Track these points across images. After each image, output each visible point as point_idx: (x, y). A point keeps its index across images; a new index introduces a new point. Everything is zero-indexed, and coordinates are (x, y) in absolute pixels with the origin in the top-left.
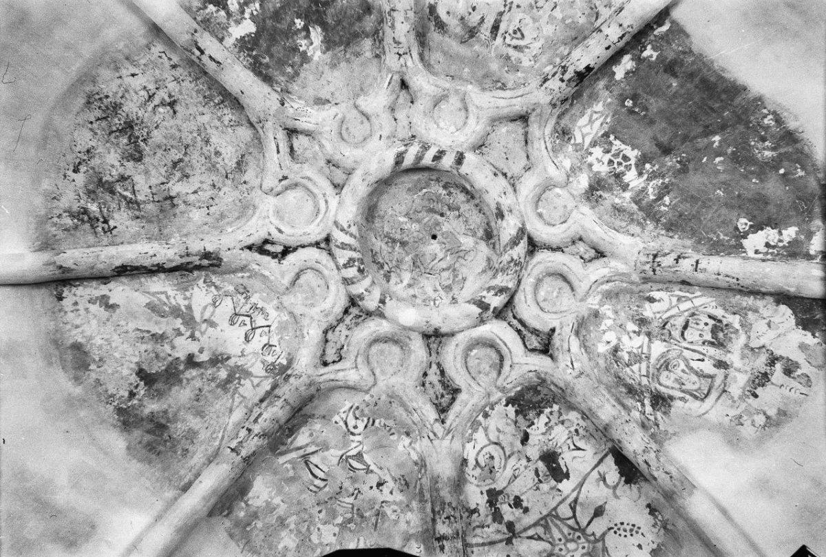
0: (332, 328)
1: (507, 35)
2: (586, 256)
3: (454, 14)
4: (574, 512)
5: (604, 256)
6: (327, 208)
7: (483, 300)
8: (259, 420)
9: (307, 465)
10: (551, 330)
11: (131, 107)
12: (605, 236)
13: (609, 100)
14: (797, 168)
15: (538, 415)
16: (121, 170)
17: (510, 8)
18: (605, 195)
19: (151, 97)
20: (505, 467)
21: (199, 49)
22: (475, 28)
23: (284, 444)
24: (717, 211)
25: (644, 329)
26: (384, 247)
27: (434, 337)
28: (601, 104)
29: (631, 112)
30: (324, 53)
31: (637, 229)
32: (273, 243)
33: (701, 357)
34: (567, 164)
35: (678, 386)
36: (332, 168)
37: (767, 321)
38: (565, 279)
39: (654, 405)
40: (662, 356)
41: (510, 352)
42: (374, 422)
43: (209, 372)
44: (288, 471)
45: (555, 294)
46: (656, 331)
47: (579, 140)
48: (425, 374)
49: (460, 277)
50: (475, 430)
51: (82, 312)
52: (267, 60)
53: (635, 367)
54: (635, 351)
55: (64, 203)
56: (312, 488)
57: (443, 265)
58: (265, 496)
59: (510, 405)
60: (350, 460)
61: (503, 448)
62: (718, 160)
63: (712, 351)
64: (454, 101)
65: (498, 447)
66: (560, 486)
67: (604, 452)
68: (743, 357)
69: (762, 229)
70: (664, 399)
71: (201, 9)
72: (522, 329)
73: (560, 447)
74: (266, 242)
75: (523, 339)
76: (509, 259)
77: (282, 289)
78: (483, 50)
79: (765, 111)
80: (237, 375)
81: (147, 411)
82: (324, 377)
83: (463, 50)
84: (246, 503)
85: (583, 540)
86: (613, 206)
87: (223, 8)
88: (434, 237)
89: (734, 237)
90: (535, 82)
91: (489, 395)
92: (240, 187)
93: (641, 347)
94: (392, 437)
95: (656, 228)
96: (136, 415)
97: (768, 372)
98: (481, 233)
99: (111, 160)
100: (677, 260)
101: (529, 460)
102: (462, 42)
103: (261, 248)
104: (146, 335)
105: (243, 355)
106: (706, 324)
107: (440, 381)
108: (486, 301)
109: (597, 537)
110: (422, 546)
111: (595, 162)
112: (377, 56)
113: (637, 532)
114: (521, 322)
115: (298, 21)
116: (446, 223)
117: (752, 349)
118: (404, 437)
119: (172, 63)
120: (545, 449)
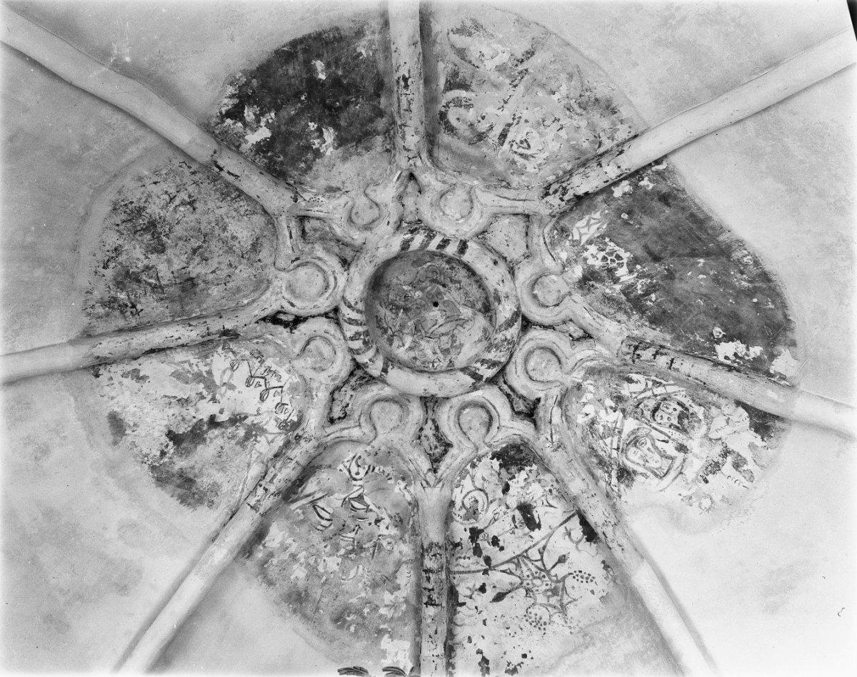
0: (338, 389)
1: (514, 143)
2: (575, 335)
3: (463, 120)
4: (542, 556)
5: (591, 338)
6: (336, 283)
7: (477, 371)
8: (275, 481)
9: (315, 509)
10: (537, 399)
11: (154, 209)
12: (593, 323)
13: (607, 211)
14: (767, 302)
15: (520, 470)
16: (146, 262)
17: (519, 121)
18: (597, 285)
19: (172, 199)
20: (487, 510)
21: (218, 167)
22: (483, 133)
23: (296, 493)
24: (697, 315)
25: (620, 406)
26: (388, 313)
27: (430, 402)
28: (598, 213)
29: (626, 223)
30: (337, 149)
31: (624, 318)
32: (285, 313)
33: (667, 438)
34: (564, 256)
35: (642, 463)
36: (341, 246)
37: (726, 418)
38: (553, 353)
39: (619, 478)
40: (633, 433)
41: (498, 415)
42: (374, 469)
43: (229, 430)
44: (299, 515)
45: (543, 365)
46: (629, 408)
47: (576, 237)
48: (421, 429)
49: (458, 343)
50: (464, 478)
51: (116, 384)
52: (282, 158)
53: (608, 441)
54: (610, 425)
55: (97, 294)
56: (319, 527)
57: (443, 330)
58: (279, 539)
59: (495, 459)
60: (352, 502)
61: (486, 494)
62: (701, 276)
63: (677, 435)
64: (460, 194)
65: (482, 493)
66: (532, 534)
67: (572, 513)
68: (702, 445)
69: (733, 341)
70: (628, 473)
71: (218, 124)
72: (511, 393)
73: (535, 502)
74: (279, 312)
75: (511, 402)
76: (503, 338)
77: (293, 356)
78: (490, 152)
79: (746, 252)
80: (254, 433)
81: (177, 468)
82: (332, 436)
83: (471, 151)
84: (264, 545)
85: (547, 579)
86: (603, 294)
87: (240, 120)
88: (436, 304)
89: (709, 340)
90: (536, 193)
91: (477, 449)
92: (255, 264)
93: (616, 422)
94: (389, 482)
95: (641, 318)
96: (168, 472)
97: (720, 462)
98: (479, 305)
99: (136, 254)
100: (655, 356)
101: (508, 507)
102: (470, 144)
103: (274, 319)
104: (173, 400)
105: (259, 414)
106: (675, 410)
107: (434, 435)
108: (480, 373)
109: (559, 579)
110: (412, 572)
111: (590, 257)
112: (388, 151)
113: (592, 581)
114: (510, 387)
115: (311, 124)
116: (448, 294)
117: (711, 439)
118: (400, 481)
119: (192, 170)
120: (522, 500)
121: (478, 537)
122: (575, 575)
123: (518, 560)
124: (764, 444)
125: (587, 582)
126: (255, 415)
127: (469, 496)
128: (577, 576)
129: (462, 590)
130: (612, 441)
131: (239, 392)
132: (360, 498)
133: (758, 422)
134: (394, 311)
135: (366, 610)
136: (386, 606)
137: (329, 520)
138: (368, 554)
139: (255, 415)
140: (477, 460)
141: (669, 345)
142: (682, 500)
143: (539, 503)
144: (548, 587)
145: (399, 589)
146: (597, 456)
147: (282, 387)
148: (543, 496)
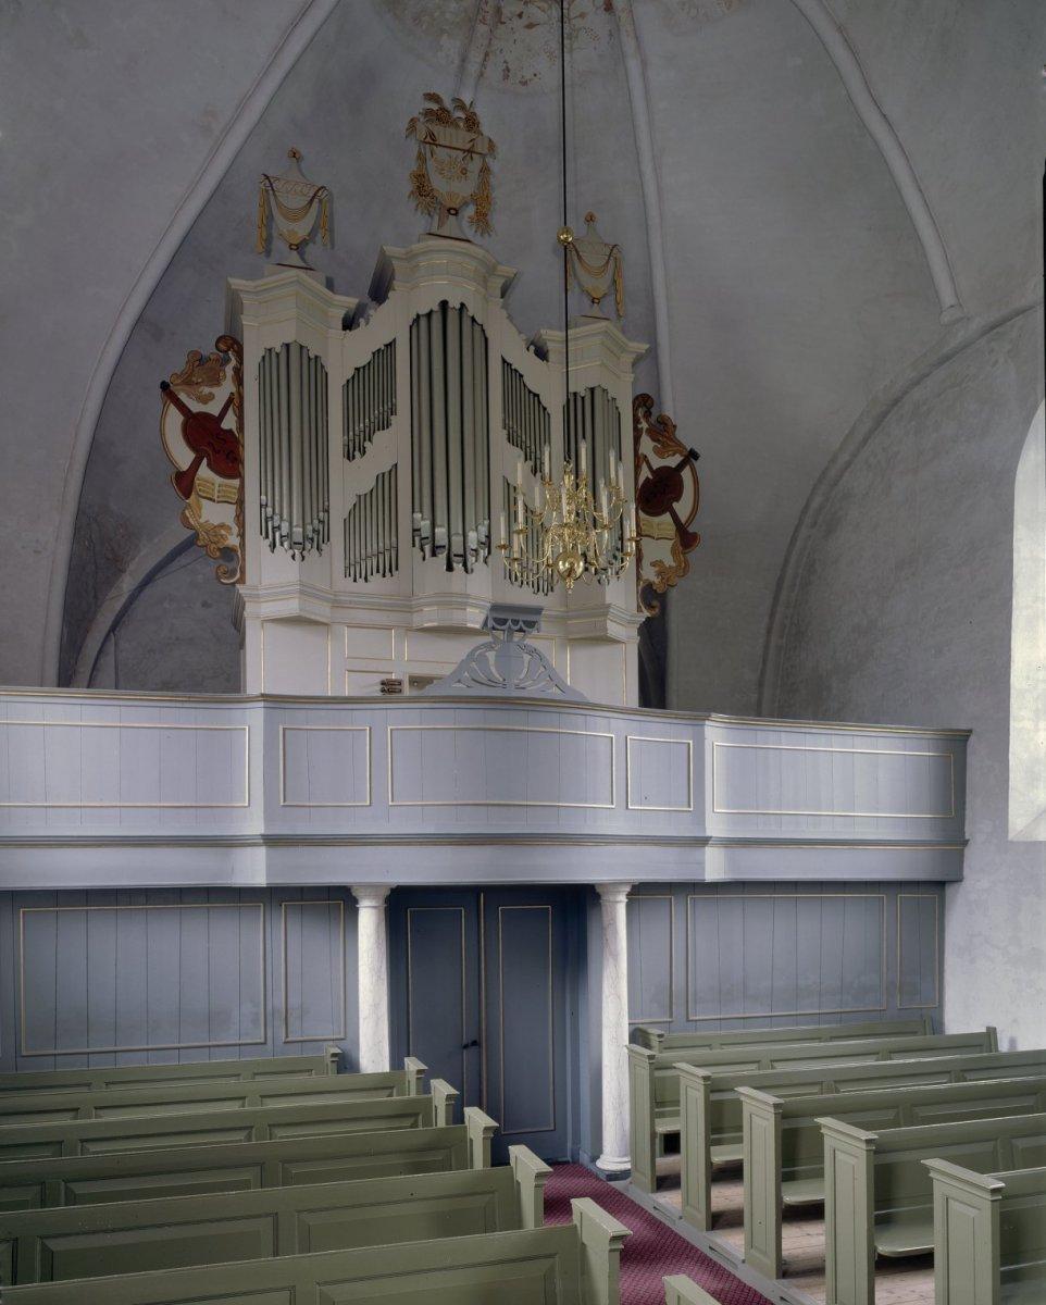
129: (506, 12)
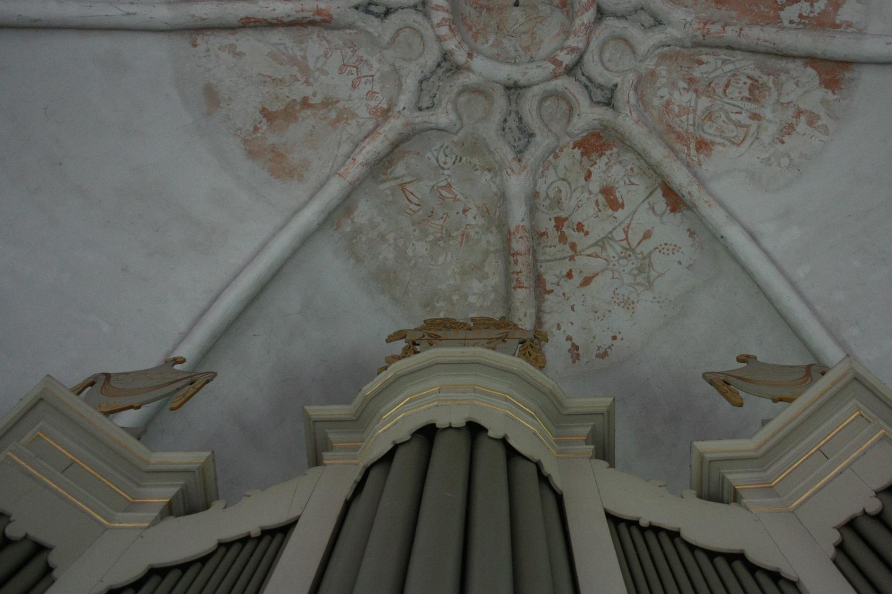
4: (627, 236)
9: (404, 191)
10: (614, 85)
15: (600, 156)
20: (570, 199)
25: (693, 87)
27: (513, 89)
33: (740, 110)
39: (698, 149)
42: (461, 159)
43: (321, 112)
48: (505, 121)
49: (538, 40)
50: (547, 169)
53: (684, 118)
54: (684, 104)
56: (408, 211)
59: (577, 148)
60: (441, 191)
61: (569, 183)
63: (749, 106)
65: (565, 183)
66: (616, 214)
68: (774, 111)
70: (706, 144)
72: (589, 84)
75: (589, 93)
80: (345, 116)
84: (352, 220)
93: (689, 101)
97: (794, 123)
101: (591, 193)
105: (350, 100)
107: (518, 127)
109: (645, 256)
110: (500, 262)
117: (782, 104)
118: (486, 173)
121: (562, 226)
122: (660, 248)
123: (601, 243)
124: (835, 97)
125: (673, 253)
126: (347, 101)
127: (554, 185)
128: (663, 249)
129: (550, 279)
130: (688, 118)
131: (332, 78)
132: (449, 186)
133: (827, 77)
134: (478, 9)
135: (455, 298)
136: (475, 294)
137: (417, 205)
138: (456, 242)
139: (347, 101)
140: (560, 151)
141: (735, 21)
142: (761, 162)
143: (622, 183)
144: (633, 266)
145: (488, 278)
146: (674, 132)
147: (372, 76)
148: (625, 175)
